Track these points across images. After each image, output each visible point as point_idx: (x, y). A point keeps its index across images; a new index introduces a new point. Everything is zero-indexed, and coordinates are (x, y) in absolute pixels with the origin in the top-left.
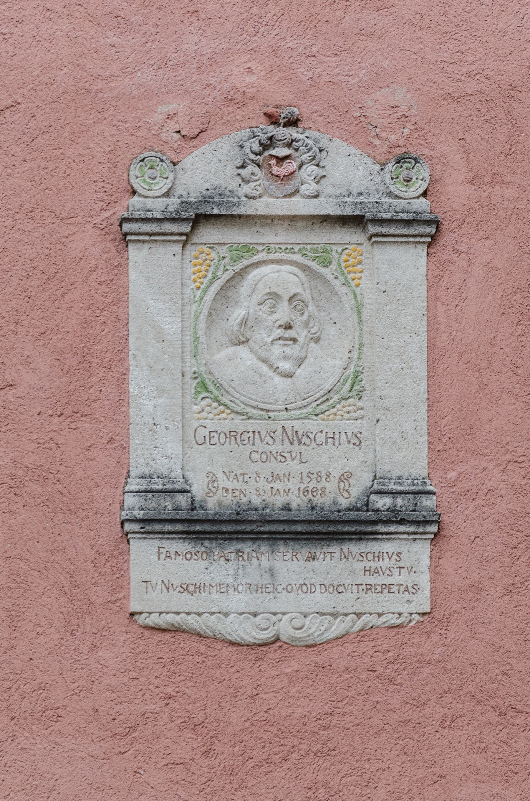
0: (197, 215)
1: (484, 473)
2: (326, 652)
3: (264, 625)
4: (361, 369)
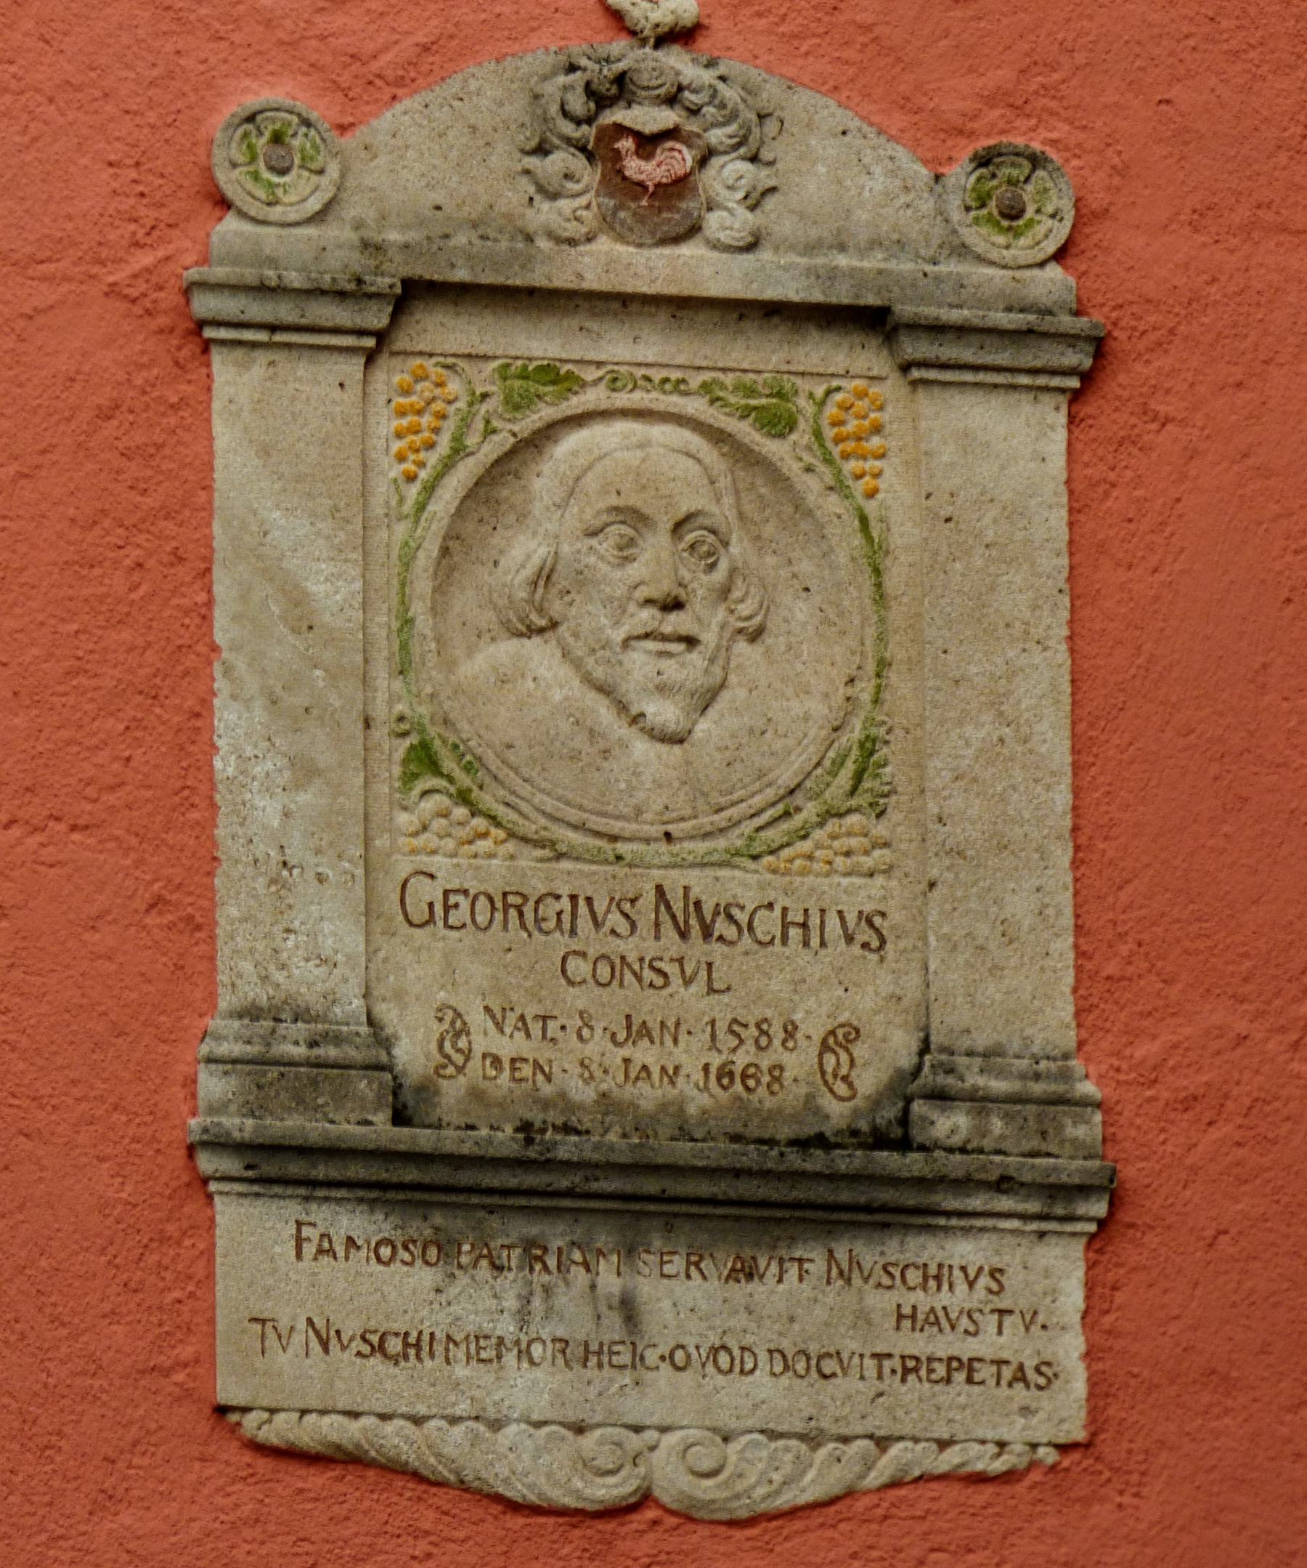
0: (406, 283)
1: (1240, 1051)
2: (788, 1545)
3: (605, 1462)
4: (882, 730)
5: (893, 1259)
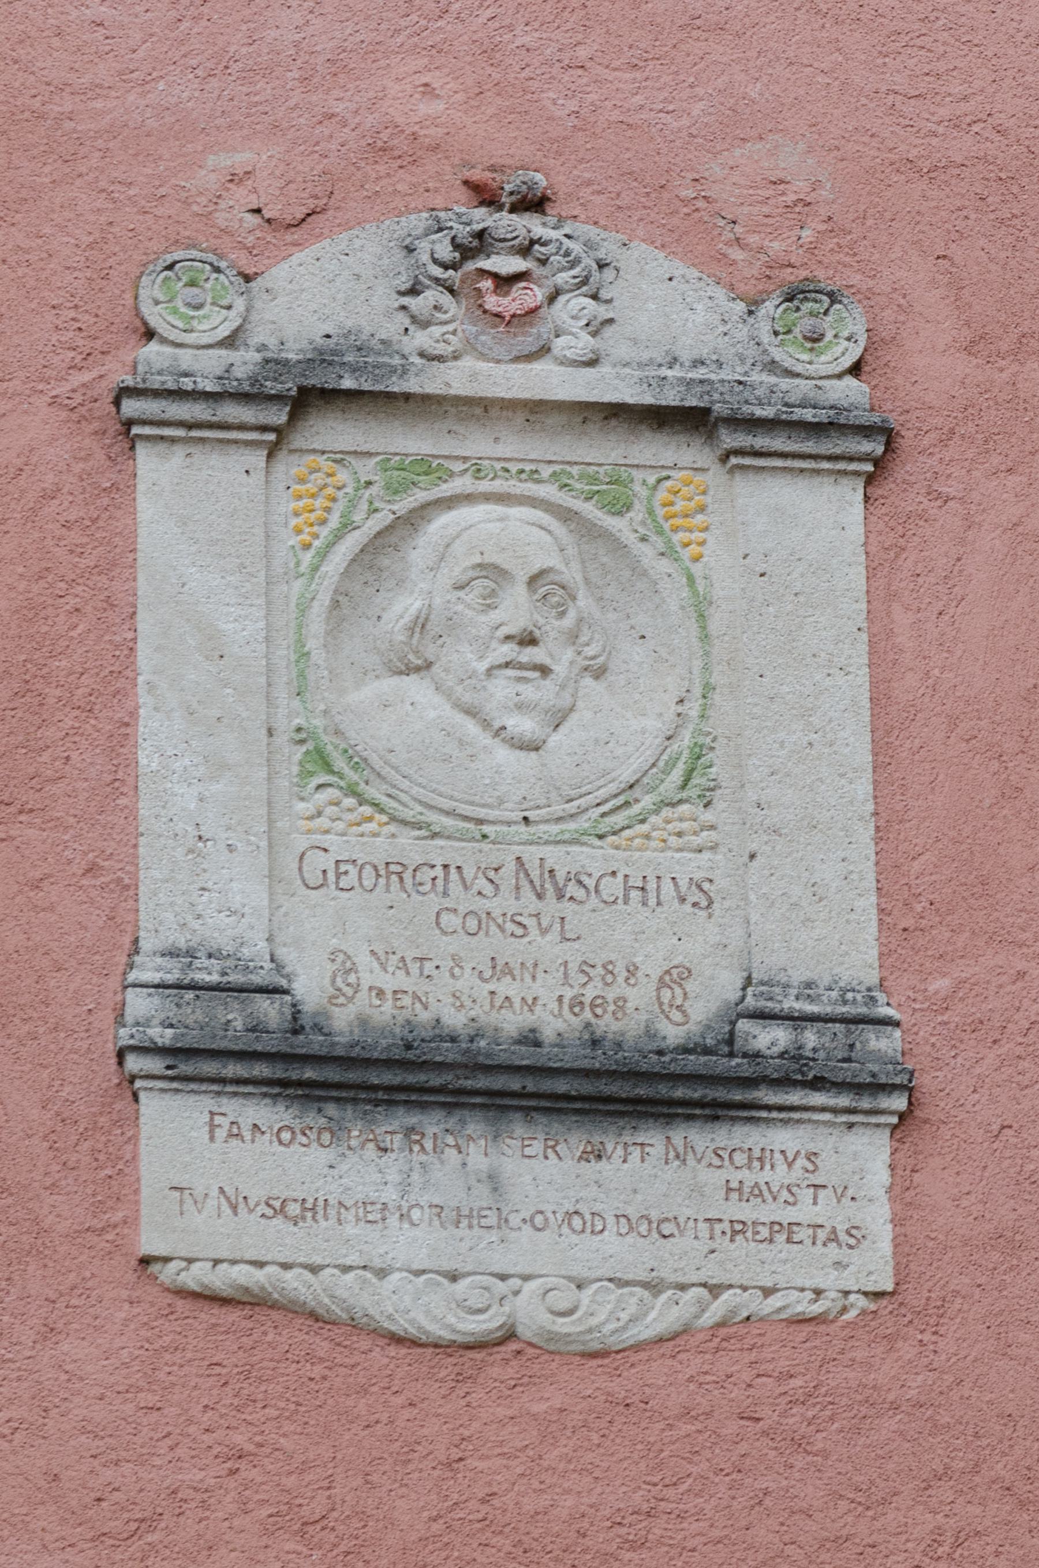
0: (303, 390)
2: (633, 1371)
4: (708, 740)
5: (722, 1145)
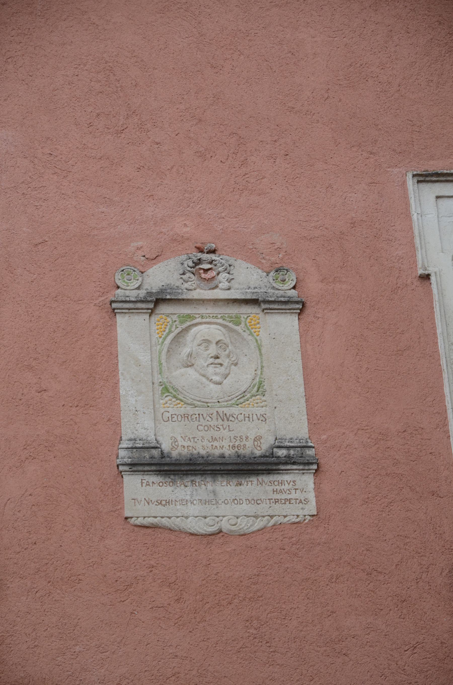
3: (211, 523)
